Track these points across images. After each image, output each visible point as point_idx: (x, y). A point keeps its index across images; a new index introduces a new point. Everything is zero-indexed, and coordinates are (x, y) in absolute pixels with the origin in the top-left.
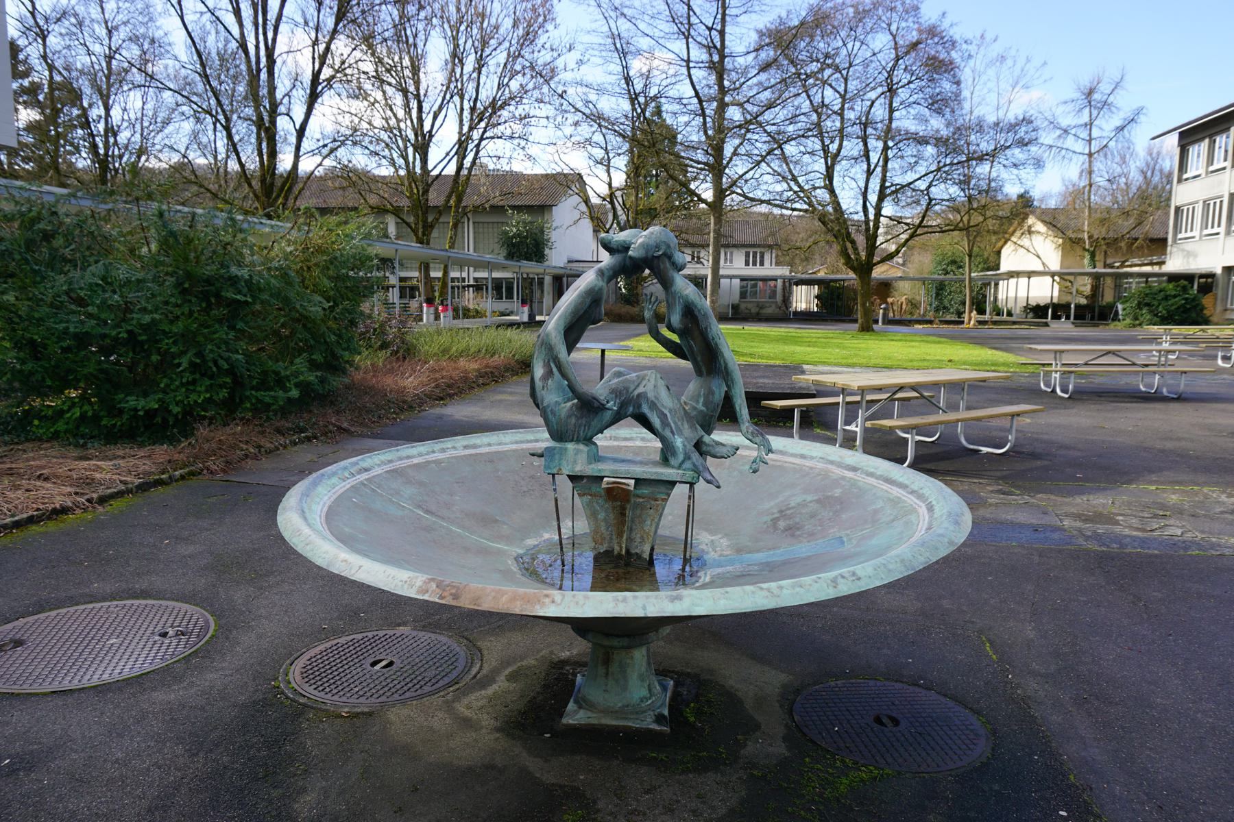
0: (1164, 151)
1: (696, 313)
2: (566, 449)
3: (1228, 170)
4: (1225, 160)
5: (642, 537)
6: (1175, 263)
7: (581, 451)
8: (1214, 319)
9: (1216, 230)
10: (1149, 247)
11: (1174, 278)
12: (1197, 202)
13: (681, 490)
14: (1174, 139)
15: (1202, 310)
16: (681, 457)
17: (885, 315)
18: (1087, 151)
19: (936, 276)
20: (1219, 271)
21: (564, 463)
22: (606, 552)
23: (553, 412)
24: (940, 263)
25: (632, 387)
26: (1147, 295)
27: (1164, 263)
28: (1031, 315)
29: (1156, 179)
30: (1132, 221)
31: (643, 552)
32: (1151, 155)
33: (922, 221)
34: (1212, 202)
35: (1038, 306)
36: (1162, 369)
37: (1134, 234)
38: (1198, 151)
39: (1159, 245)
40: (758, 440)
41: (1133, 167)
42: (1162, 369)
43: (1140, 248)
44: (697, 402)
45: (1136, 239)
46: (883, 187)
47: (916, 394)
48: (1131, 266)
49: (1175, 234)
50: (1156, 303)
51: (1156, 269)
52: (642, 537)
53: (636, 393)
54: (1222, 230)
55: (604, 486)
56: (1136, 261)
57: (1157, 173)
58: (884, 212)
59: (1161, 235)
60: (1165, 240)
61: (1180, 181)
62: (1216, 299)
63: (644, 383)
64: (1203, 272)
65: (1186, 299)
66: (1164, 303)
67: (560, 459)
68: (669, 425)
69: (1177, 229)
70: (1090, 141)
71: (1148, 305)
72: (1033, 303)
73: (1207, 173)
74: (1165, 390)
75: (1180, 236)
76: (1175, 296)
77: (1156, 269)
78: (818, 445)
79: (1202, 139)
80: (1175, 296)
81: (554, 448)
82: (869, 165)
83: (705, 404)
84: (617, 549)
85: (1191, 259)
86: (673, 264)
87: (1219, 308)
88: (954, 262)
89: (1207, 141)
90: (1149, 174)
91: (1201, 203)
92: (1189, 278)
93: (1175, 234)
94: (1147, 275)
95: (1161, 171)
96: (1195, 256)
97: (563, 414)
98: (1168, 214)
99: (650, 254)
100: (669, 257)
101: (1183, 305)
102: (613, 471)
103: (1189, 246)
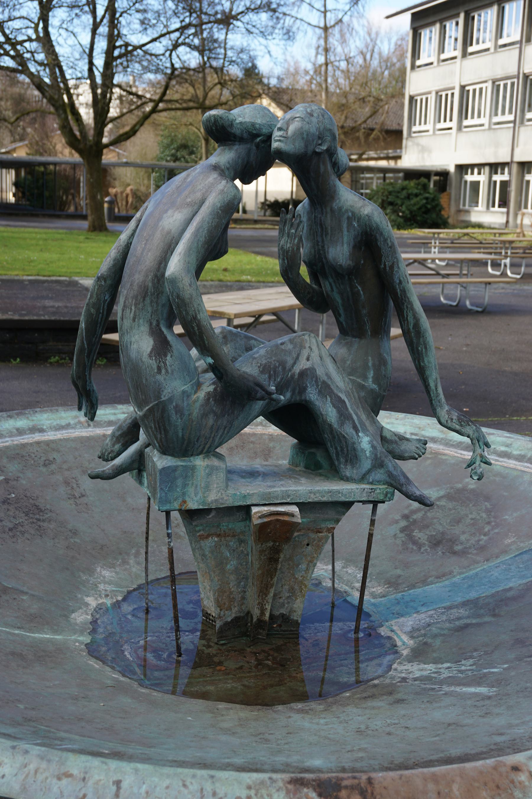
0: (382, 32)
1: (381, 243)
2: (193, 468)
3: (458, 60)
4: (455, 49)
5: (292, 590)
6: (411, 158)
7: (217, 469)
8: (450, 221)
9: (448, 124)
10: (385, 139)
11: (411, 174)
12: (430, 93)
13: (360, 513)
14: (408, 16)
15: (440, 211)
16: (367, 465)
17: (111, 210)
18: (322, 25)
19: (164, 163)
20: (452, 169)
21: (191, 490)
22: (237, 619)
23: (179, 410)
24: (168, 146)
25: (290, 361)
26: (390, 193)
27: (399, 157)
28: (268, 212)
29: (375, 63)
30: (367, 110)
31: (292, 611)
32: (369, 34)
33: (164, 94)
34: (444, 94)
35: (276, 203)
36: (464, 280)
37: (371, 123)
38: (430, 36)
39: (394, 137)
40: (469, 430)
41: (353, 46)
42: (464, 280)
43: (377, 139)
44: (365, 378)
45: (372, 130)
46: (111, 47)
47: (274, 317)
48: (368, 159)
49: (410, 127)
50: (399, 202)
51: (392, 164)
52: (292, 590)
53: (297, 369)
54: (454, 124)
55: (256, 521)
56: (372, 154)
57: (376, 55)
58: (68, 77)
59: (395, 127)
60: (399, 133)
61: (413, 67)
62: (450, 199)
63: (305, 353)
64: (439, 169)
65: (427, 198)
66: (407, 203)
67: (185, 485)
68: (349, 417)
69: (411, 122)
70: (325, 12)
71: (391, 204)
72: (271, 198)
73: (439, 60)
74: (468, 303)
75: (414, 129)
76: (416, 195)
77: (392, 164)
78: (401, 415)
79: (433, 23)
80: (416, 195)
81: (174, 469)
82: (95, 17)
83: (376, 380)
84: (256, 612)
85: (426, 155)
86: (335, 165)
87: (453, 209)
88: (184, 146)
89: (438, 26)
90: (368, 57)
91: (433, 95)
92: (425, 174)
93: (410, 127)
94: (384, 171)
95: (380, 54)
96: (430, 151)
97: (196, 412)
98: (403, 105)
99: (311, 149)
100: (331, 153)
101: (424, 206)
102: (264, 496)
103: (423, 141)
